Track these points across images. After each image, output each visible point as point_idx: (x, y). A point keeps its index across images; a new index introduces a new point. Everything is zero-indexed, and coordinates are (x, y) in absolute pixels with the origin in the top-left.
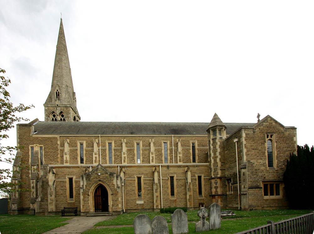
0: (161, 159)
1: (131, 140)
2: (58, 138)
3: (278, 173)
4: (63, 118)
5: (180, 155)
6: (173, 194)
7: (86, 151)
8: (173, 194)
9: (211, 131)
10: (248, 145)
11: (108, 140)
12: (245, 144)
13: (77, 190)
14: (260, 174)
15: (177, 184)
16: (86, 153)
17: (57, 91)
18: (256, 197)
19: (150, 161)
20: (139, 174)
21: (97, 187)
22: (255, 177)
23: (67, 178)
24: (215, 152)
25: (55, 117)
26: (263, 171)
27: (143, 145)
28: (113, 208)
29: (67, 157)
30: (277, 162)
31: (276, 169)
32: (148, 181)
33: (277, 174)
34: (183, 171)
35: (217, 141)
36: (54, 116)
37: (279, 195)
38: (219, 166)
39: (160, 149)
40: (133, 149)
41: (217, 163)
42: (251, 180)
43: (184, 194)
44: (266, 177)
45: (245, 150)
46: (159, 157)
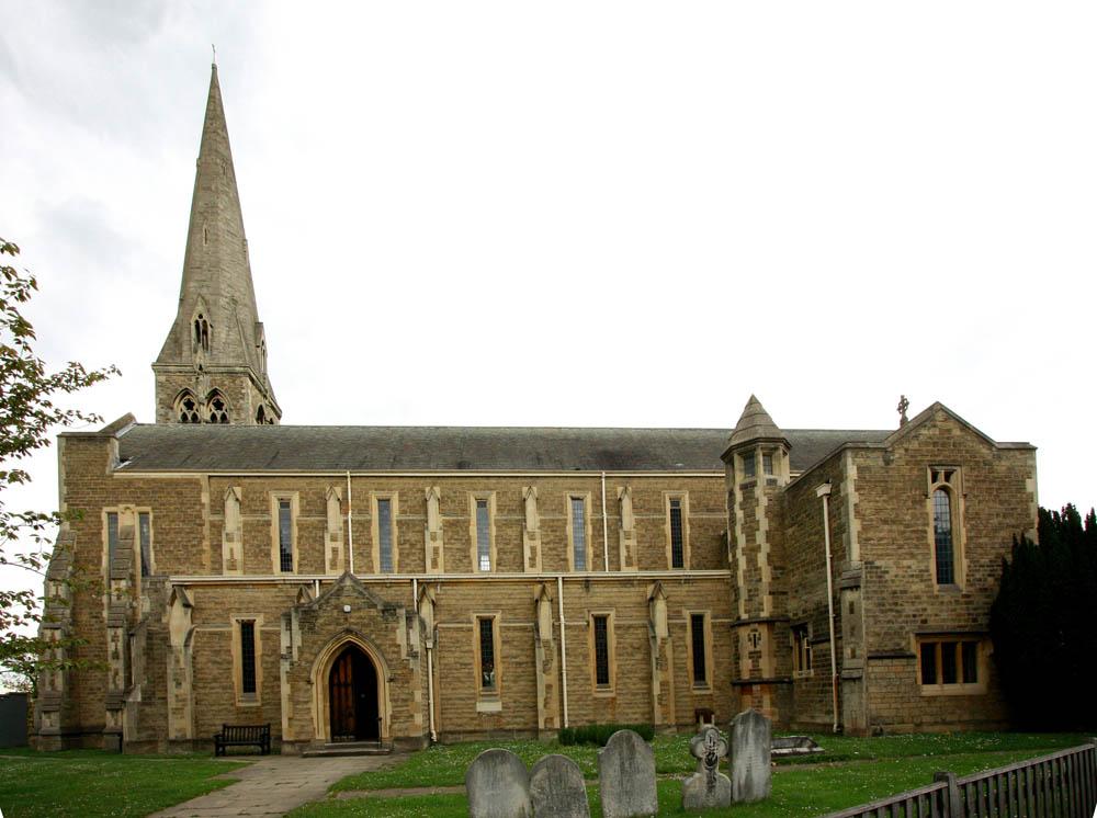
1: (459, 488)
2: (204, 483)
4: (219, 414)
5: (628, 542)
6: (603, 677)
7: (300, 530)
8: (603, 677)
10: (868, 508)
11: (376, 490)
12: (855, 505)
13: (270, 666)
14: (909, 609)
15: (619, 643)
17: (201, 316)
18: (895, 689)
19: (523, 563)
20: (487, 608)
21: (337, 654)
22: (890, 618)
23: (233, 621)
26: (917, 597)
27: (498, 505)
28: (396, 726)
29: (233, 549)
30: (969, 566)
32: (516, 634)
33: (968, 609)
34: (639, 599)
35: (759, 492)
36: (189, 405)
37: (974, 680)
38: (764, 580)
39: (558, 520)
40: (464, 522)
41: (757, 569)
43: (642, 679)
44: (928, 618)
45: (855, 526)
46: (554, 549)
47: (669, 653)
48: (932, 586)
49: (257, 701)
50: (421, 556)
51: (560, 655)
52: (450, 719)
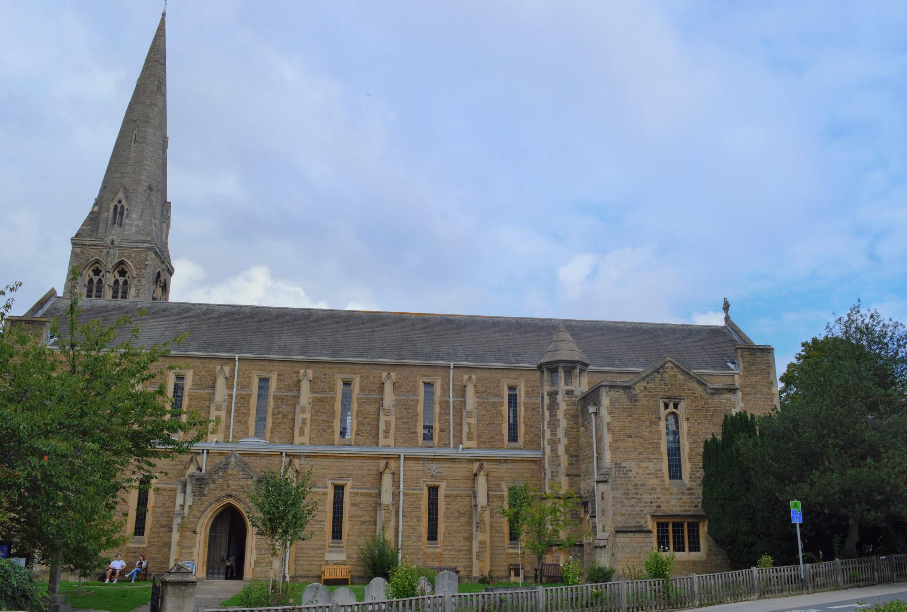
0: (413, 430)
3: (694, 496)
4: (122, 280)
5: (469, 421)
6: (433, 535)
7: (190, 399)
8: (433, 535)
9: (545, 370)
12: (608, 424)
13: (158, 515)
14: (647, 497)
15: (447, 508)
16: (191, 403)
17: (120, 202)
18: (637, 555)
19: (378, 434)
21: (219, 511)
24: (554, 426)
25: (99, 275)
26: (653, 489)
27: (361, 386)
28: (258, 569)
30: (691, 468)
31: (688, 486)
32: (362, 498)
33: (691, 498)
34: (466, 474)
35: (560, 398)
36: (97, 272)
37: (698, 549)
38: (562, 465)
40: (331, 398)
41: (558, 457)
42: (623, 512)
43: (465, 538)
44: (662, 505)
45: (607, 438)
46: (406, 423)
47: (487, 519)
48: (664, 481)
49: (144, 543)
50: (291, 426)
51: (397, 515)
52: (302, 565)
